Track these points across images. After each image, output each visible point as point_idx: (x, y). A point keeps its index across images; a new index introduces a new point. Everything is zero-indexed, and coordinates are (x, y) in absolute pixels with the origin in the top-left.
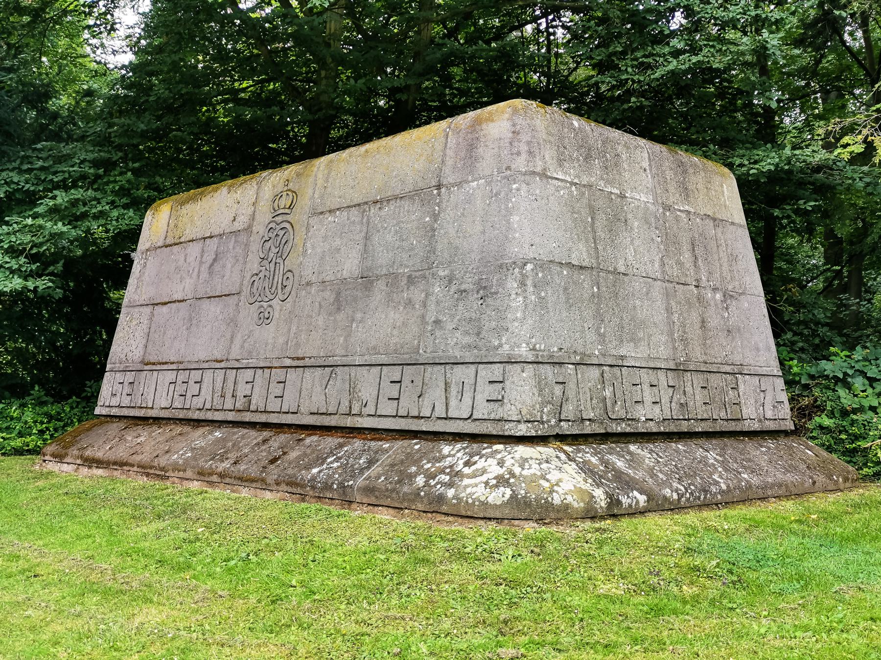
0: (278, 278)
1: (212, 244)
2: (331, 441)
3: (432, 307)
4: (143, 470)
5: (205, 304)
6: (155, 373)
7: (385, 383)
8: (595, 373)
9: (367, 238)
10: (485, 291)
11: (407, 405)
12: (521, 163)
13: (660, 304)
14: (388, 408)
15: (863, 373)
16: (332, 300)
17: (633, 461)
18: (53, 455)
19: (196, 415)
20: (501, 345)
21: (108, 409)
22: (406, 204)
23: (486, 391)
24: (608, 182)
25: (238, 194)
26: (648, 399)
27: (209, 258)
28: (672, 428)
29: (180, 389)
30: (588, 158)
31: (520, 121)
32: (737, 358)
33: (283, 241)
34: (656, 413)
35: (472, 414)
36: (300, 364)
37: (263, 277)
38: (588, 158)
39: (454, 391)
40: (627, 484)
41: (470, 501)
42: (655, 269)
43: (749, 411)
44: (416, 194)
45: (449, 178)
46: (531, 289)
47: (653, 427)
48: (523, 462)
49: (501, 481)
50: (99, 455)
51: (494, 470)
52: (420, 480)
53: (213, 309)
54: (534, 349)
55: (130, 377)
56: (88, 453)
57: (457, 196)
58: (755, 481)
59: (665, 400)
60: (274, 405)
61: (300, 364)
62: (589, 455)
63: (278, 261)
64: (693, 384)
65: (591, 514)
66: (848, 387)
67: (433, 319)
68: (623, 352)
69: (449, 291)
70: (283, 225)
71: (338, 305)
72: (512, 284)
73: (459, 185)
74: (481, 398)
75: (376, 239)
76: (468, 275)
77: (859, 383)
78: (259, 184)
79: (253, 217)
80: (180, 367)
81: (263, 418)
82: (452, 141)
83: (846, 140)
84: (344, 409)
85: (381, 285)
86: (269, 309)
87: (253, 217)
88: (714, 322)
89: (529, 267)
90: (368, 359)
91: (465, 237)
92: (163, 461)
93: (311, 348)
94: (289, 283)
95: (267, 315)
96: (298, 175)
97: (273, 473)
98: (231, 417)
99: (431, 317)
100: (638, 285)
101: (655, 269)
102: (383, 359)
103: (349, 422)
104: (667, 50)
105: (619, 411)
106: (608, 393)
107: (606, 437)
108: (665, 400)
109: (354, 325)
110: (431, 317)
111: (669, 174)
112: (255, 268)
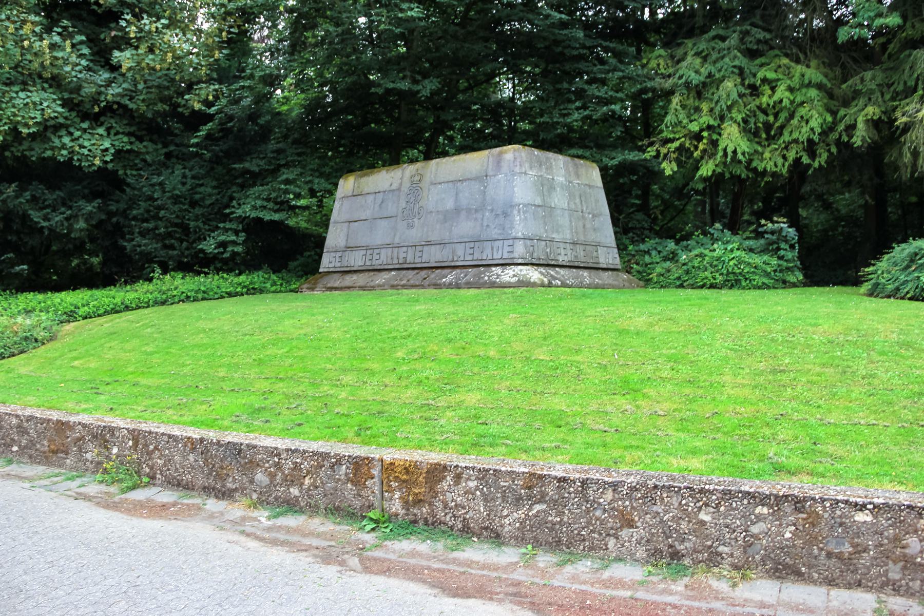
0: (416, 210)
1: (380, 196)
2: (448, 271)
3: (485, 220)
5: (379, 221)
7: (467, 249)
8: (544, 243)
9: (457, 194)
10: (506, 214)
11: (476, 256)
12: (517, 170)
13: (567, 219)
15: (656, 249)
17: (557, 273)
18: (308, 288)
19: (379, 267)
22: (473, 182)
23: (507, 249)
24: (548, 174)
25: (392, 174)
26: (563, 252)
27: (379, 201)
28: (571, 264)
29: (369, 257)
30: (540, 166)
31: (517, 154)
32: (598, 240)
34: (566, 258)
36: (429, 244)
38: (540, 166)
39: (495, 250)
40: (555, 279)
42: (565, 206)
43: (602, 260)
44: (477, 179)
45: (490, 173)
47: (564, 263)
49: (514, 276)
50: (336, 285)
51: (511, 273)
52: (486, 278)
53: (384, 223)
55: (339, 254)
56: (329, 285)
57: (494, 180)
58: (600, 282)
59: (569, 254)
60: (419, 260)
61: (429, 244)
62: (542, 269)
64: (580, 249)
65: (543, 285)
66: (650, 255)
68: (553, 236)
71: (445, 220)
72: (515, 212)
73: (495, 176)
74: (505, 251)
75: (461, 195)
77: (654, 253)
78: (403, 170)
79: (401, 184)
80: (367, 248)
81: (413, 266)
82: (491, 159)
83: (649, 149)
84: (451, 258)
85: (464, 213)
87: (401, 184)
88: (588, 226)
90: (460, 240)
92: (372, 284)
93: (434, 237)
94: (422, 212)
96: (423, 167)
97: (426, 282)
98: (397, 266)
99: (485, 224)
100: (559, 211)
101: (565, 206)
102: (466, 240)
103: (453, 264)
104: (573, 107)
105: (552, 256)
106: (548, 250)
107: (548, 265)
108: (569, 254)
110: (485, 224)
111: (571, 169)
112: (404, 205)
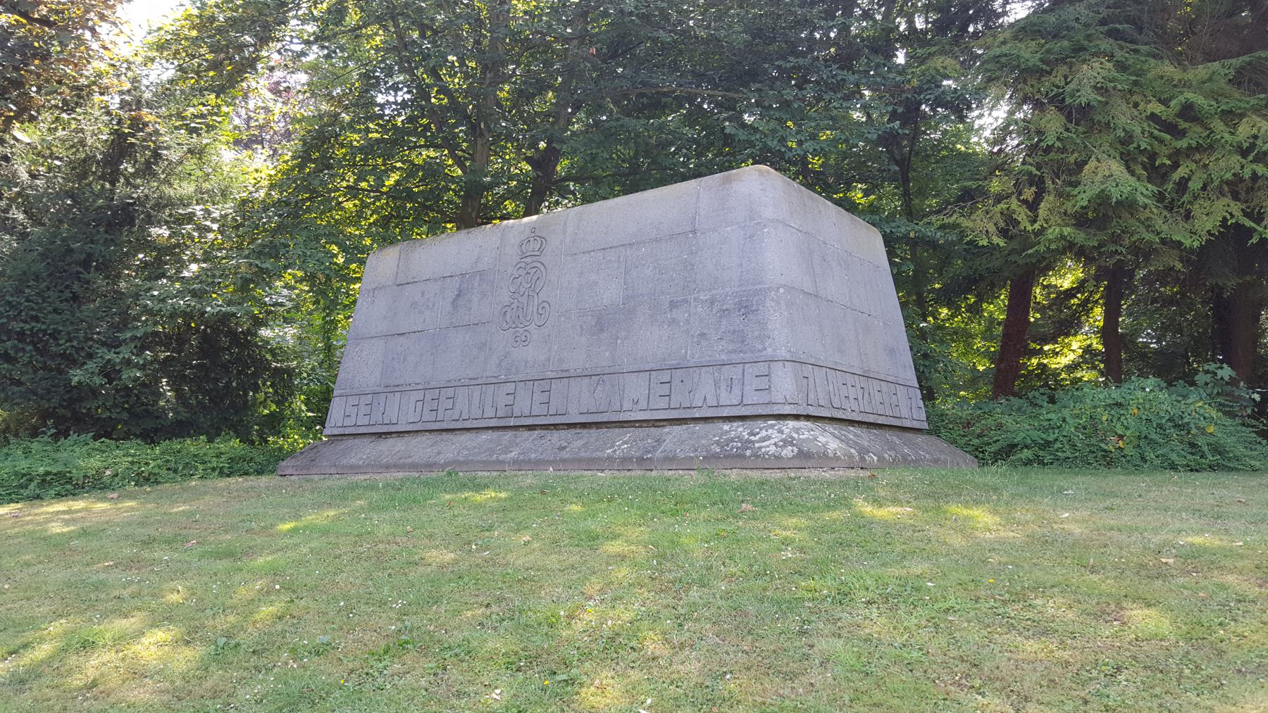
4: (75, 516)
6: (398, 395)
11: (376, 417)
14: (663, 403)
16: (593, 323)
20: (765, 349)
21: (340, 429)
33: (535, 278)
35: (742, 402)
37: (515, 308)
41: (767, 457)
46: (784, 306)
48: (797, 430)
54: (790, 351)
63: (531, 293)
67: (698, 332)
69: (711, 311)
70: (533, 265)
76: (729, 298)
86: (526, 333)
89: (782, 290)
91: (724, 269)
95: (523, 339)
98: (493, 423)
103: (622, 417)
109: (619, 341)
